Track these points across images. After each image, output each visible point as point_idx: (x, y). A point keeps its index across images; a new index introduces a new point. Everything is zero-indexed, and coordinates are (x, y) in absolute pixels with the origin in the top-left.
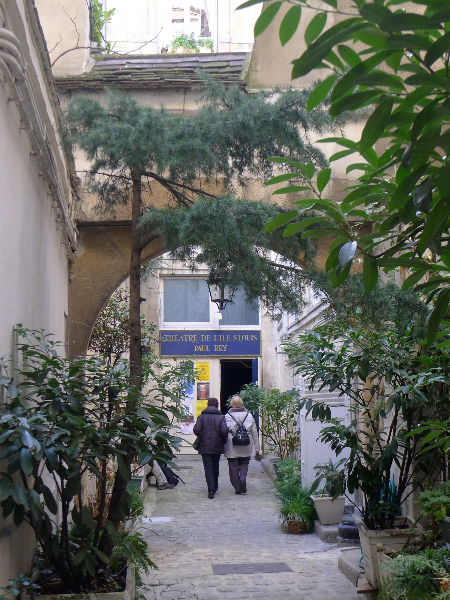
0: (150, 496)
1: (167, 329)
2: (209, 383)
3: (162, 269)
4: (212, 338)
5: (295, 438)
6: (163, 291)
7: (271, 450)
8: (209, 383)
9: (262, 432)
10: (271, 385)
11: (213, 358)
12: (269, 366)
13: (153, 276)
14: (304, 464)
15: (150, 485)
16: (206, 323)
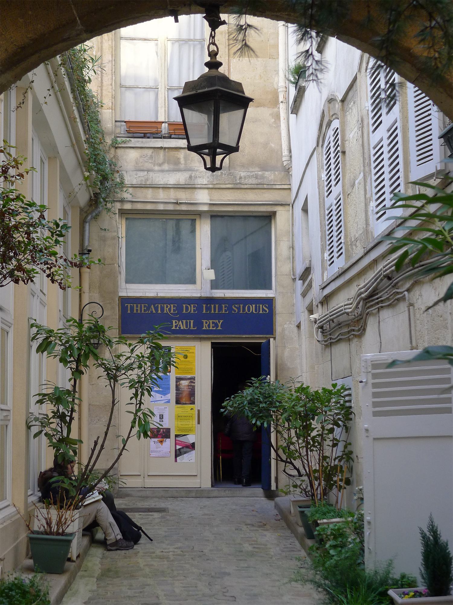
0: (90, 564)
1: (131, 294)
2: (194, 378)
3: (122, 201)
4: (200, 309)
5: (336, 466)
6: (124, 235)
7: (295, 486)
8: (194, 378)
9: (276, 451)
10: (292, 380)
11: (201, 339)
12: (287, 353)
13: (109, 210)
14: (369, 523)
15: (94, 542)
16: (190, 287)
